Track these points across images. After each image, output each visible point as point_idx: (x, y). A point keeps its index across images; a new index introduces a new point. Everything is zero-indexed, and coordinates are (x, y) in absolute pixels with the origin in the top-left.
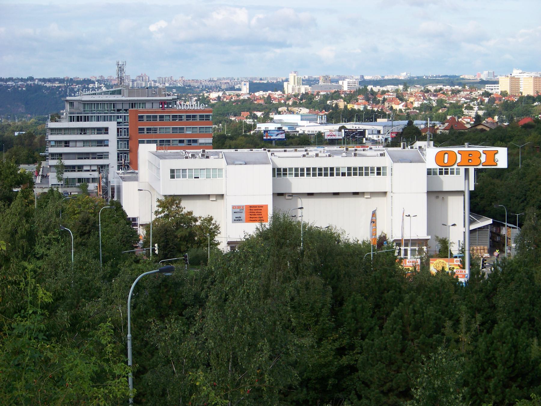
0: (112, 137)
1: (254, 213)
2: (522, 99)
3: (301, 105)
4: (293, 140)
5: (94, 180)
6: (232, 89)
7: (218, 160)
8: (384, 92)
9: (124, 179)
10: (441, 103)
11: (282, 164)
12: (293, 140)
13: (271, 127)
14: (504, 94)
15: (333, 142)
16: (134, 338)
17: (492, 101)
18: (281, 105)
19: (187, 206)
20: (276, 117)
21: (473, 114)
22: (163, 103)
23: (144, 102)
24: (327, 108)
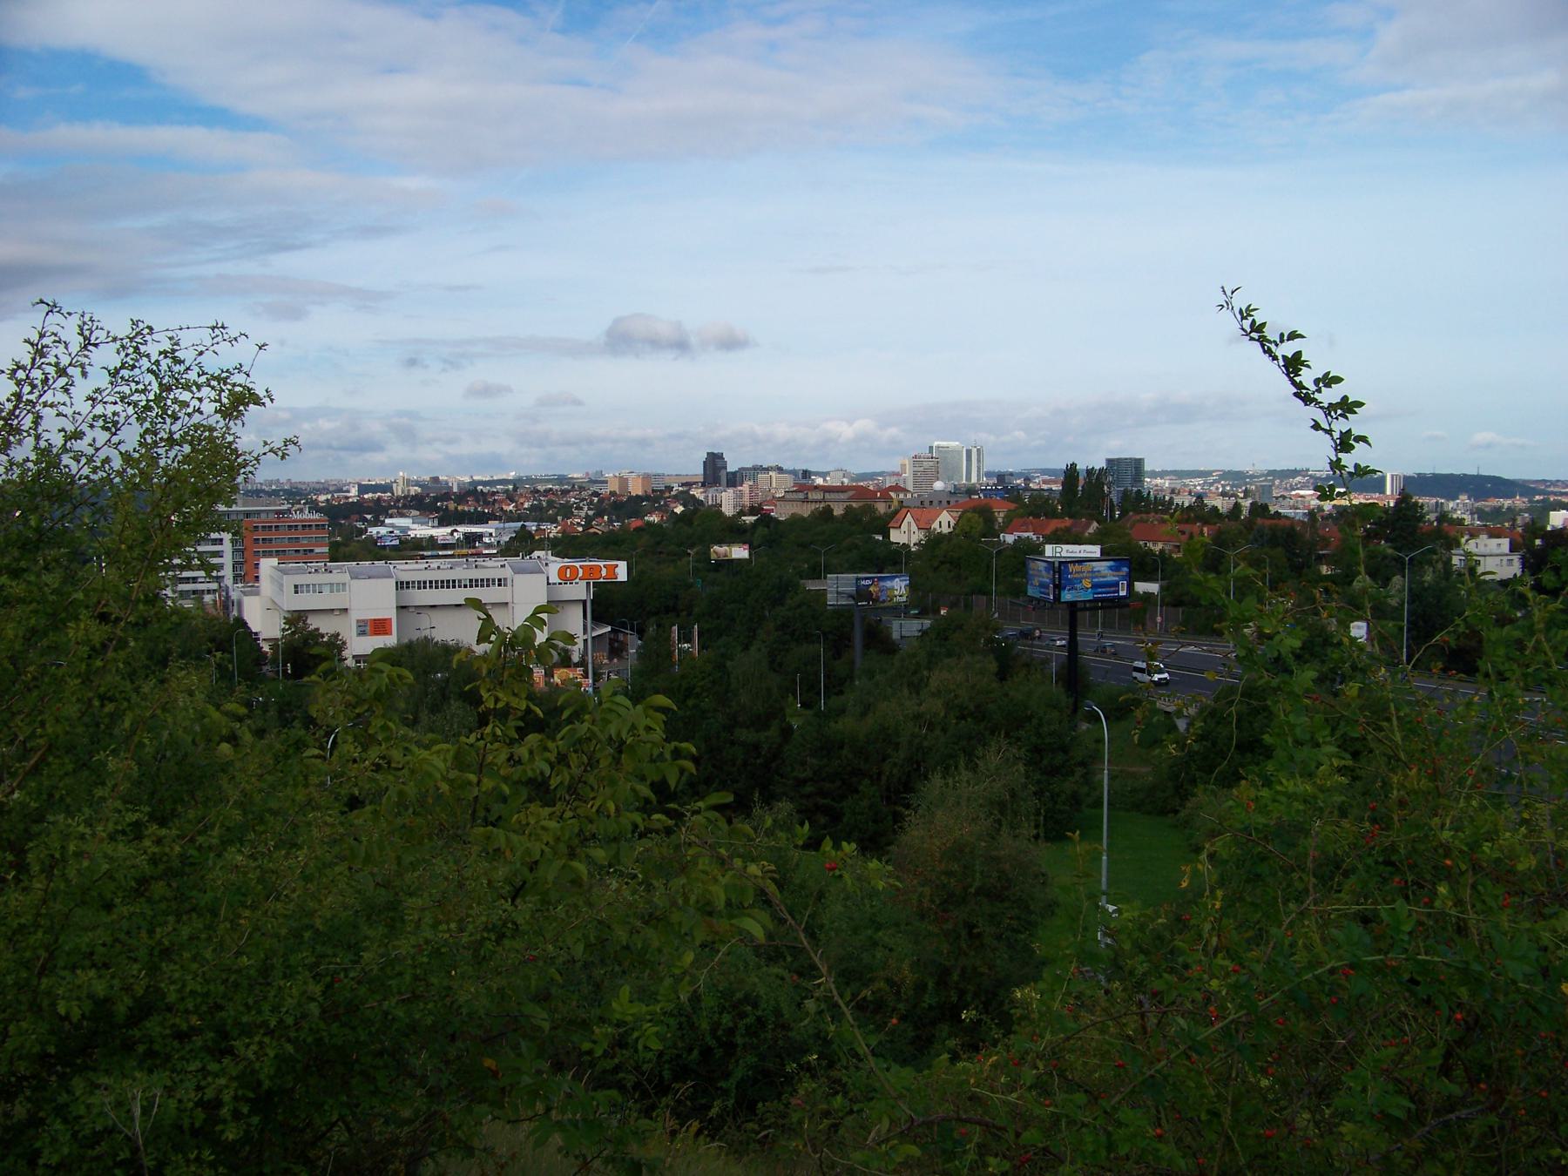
0: (227, 547)
1: (380, 627)
2: (631, 498)
3: (411, 507)
4: (411, 548)
5: (209, 592)
6: (341, 491)
7: (341, 572)
8: (494, 494)
9: (245, 594)
10: (551, 504)
11: (405, 577)
12: (411, 548)
13: (383, 531)
14: (613, 494)
15: (445, 547)
16: (1112, 778)
17: (601, 501)
18: (391, 507)
19: (314, 623)
20: (388, 521)
21: (583, 514)
22: (278, 512)
23: (259, 512)
24: (438, 510)
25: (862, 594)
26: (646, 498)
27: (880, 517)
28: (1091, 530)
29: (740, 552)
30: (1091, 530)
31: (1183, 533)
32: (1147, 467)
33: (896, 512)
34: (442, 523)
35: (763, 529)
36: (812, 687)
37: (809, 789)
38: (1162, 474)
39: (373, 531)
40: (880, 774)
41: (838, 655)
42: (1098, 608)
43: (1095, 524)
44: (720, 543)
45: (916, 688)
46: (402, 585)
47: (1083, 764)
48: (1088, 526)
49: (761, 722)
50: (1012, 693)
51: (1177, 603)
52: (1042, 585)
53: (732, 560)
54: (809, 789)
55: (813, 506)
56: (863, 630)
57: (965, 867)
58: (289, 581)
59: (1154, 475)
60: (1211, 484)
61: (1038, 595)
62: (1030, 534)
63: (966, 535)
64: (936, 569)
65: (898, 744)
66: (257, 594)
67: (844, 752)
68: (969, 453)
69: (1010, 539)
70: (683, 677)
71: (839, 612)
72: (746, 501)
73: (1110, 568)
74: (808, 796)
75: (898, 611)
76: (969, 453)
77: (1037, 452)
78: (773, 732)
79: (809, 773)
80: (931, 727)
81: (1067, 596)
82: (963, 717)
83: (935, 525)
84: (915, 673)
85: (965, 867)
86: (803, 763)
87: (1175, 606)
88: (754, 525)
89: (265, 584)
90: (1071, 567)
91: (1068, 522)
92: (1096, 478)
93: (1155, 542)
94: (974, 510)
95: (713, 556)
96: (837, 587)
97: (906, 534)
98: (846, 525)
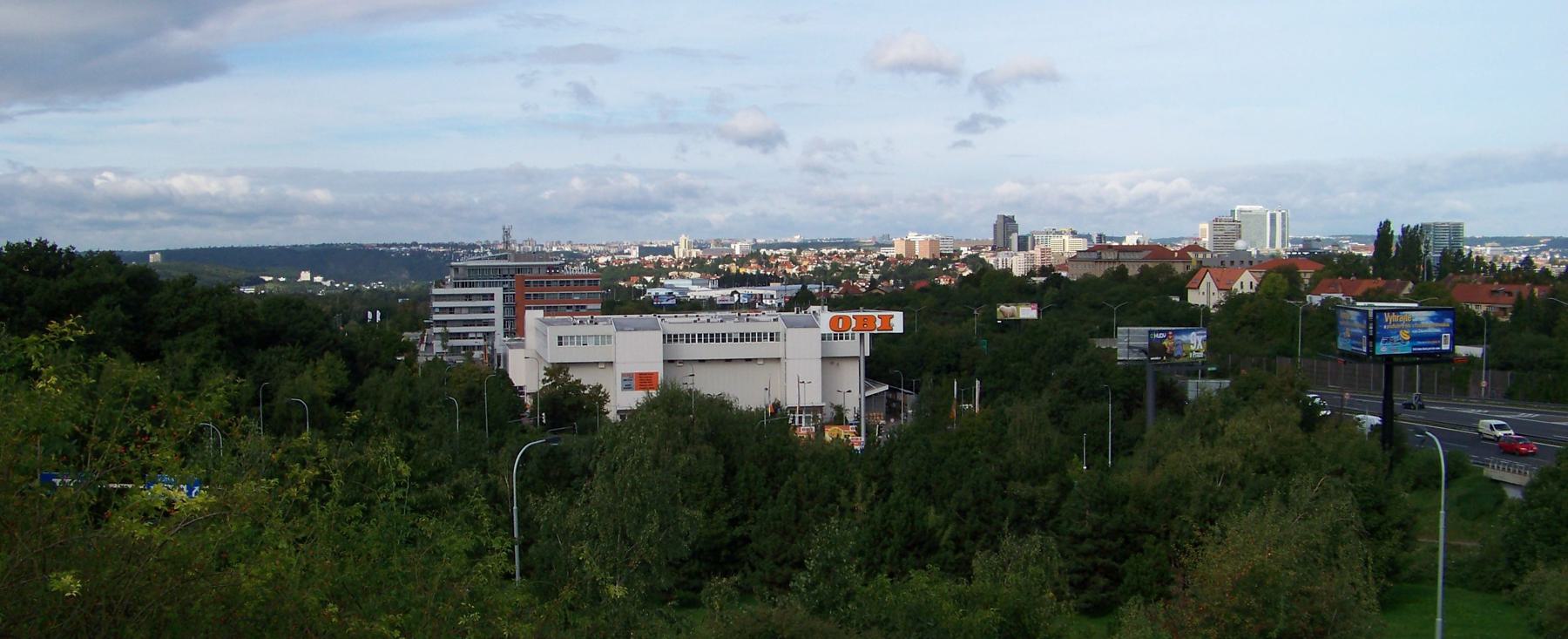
1: (644, 380)
2: (917, 261)
3: (692, 269)
5: (479, 348)
7: (606, 325)
9: (511, 347)
10: (835, 266)
13: (662, 292)
14: (899, 257)
17: (887, 264)
18: (671, 269)
19: (575, 375)
21: (868, 277)
22: (550, 268)
23: (531, 268)
24: (719, 272)
25: (1155, 348)
26: (934, 261)
27: (1177, 278)
28: (1406, 291)
29: (1028, 312)
30: (1406, 291)
31: (1510, 294)
32: (1467, 234)
33: (1195, 272)
34: (722, 284)
35: (1049, 286)
36: (1099, 448)
37: (1087, 546)
38: (1483, 241)
39: (652, 292)
40: (1167, 533)
41: (1129, 414)
42: (1415, 363)
43: (1411, 285)
44: (1007, 302)
45: (1209, 437)
46: (669, 339)
47: (1401, 526)
48: (1403, 286)
49: (1036, 475)
50: (1320, 444)
51: (1505, 367)
52: (1355, 337)
53: (1019, 321)
54: (1087, 546)
55: (1107, 266)
56: (1158, 387)
57: (1266, 604)
58: (553, 333)
59: (1474, 241)
60: (1538, 252)
61: (1349, 348)
62: (1339, 295)
63: (1270, 296)
64: (1237, 330)
65: (1189, 499)
66: (523, 347)
67: (1128, 507)
68: (1273, 217)
69: (1316, 300)
70: (960, 434)
71: (1132, 369)
72: (1038, 263)
73: (1432, 318)
74: (1086, 555)
75: (1193, 369)
76: (1273, 217)
77: (1349, 226)
78: (1050, 487)
79: (1087, 528)
80: (1227, 479)
81: (1382, 349)
82: (1264, 471)
83: (1236, 286)
84: (1208, 423)
85: (1266, 604)
86: (1082, 517)
87: (1502, 369)
88: (1044, 286)
89: (530, 337)
90: (1387, 317)
91: (1380, 282)
92: (1412, 237)
93: (1478, 304)
94: (1279, 270)
95: (1000, 316)
96: (1129, 341)
97: (1205, 295)
98: (1143, 283)
